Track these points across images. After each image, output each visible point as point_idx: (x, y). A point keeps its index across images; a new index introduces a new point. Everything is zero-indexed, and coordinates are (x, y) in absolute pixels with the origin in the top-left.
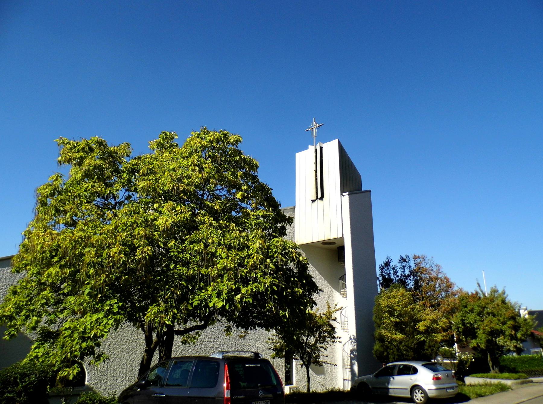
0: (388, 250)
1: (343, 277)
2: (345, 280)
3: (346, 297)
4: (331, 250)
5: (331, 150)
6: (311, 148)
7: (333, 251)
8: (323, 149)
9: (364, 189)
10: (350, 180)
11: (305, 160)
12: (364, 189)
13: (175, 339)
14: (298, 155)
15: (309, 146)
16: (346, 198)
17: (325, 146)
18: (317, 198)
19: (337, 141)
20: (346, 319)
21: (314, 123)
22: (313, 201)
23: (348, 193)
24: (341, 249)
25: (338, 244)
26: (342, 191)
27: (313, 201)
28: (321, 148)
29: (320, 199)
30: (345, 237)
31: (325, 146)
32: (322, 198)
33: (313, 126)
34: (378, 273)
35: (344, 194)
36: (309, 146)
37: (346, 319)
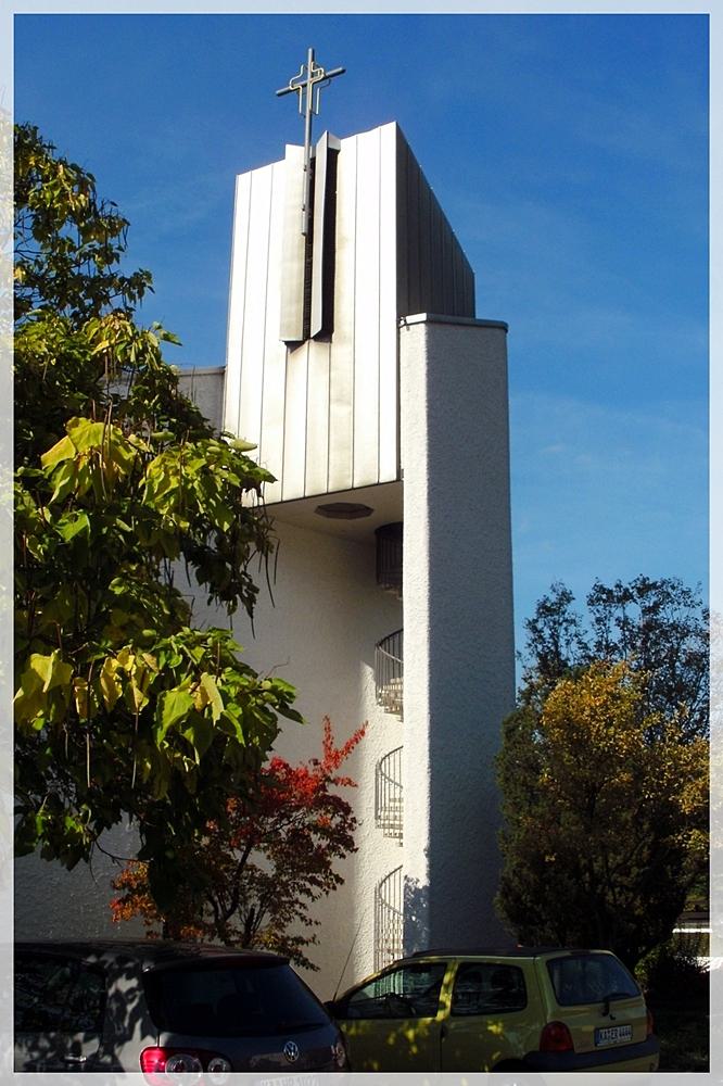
0: (560, 554)
1: (392, 639)
2: (398, 650)
3: (400, 711)
4: (291, 352)
5: (370, 163)
6: (295, 155)
7: (359, 531)
8: (340, 157)
9: (480, 315)
10: (432, 275)
11: (267, 198)
12: (480, 315)
13: (654, 1056)
14: (243, 181)
15: (289, 147)
16: (417, 334)
17: (347, 146)
18: (307, 335)
19: (388, 132)
20: (393, 792)
21: (310, 64)
22: (293, 346)
23: (423, 317)
24: (391, 534)
25: (378, 518)
26: (405, 307)
27: (293, 346)
28: (332, 155)
29: (318, 338)
30: (405, 479)
31: (347, 146)
32: (326, 334)
33: (304, 77)
34: (522, 637)
35: (410, 319)
36: (289, 147)
37: (393, 792)
